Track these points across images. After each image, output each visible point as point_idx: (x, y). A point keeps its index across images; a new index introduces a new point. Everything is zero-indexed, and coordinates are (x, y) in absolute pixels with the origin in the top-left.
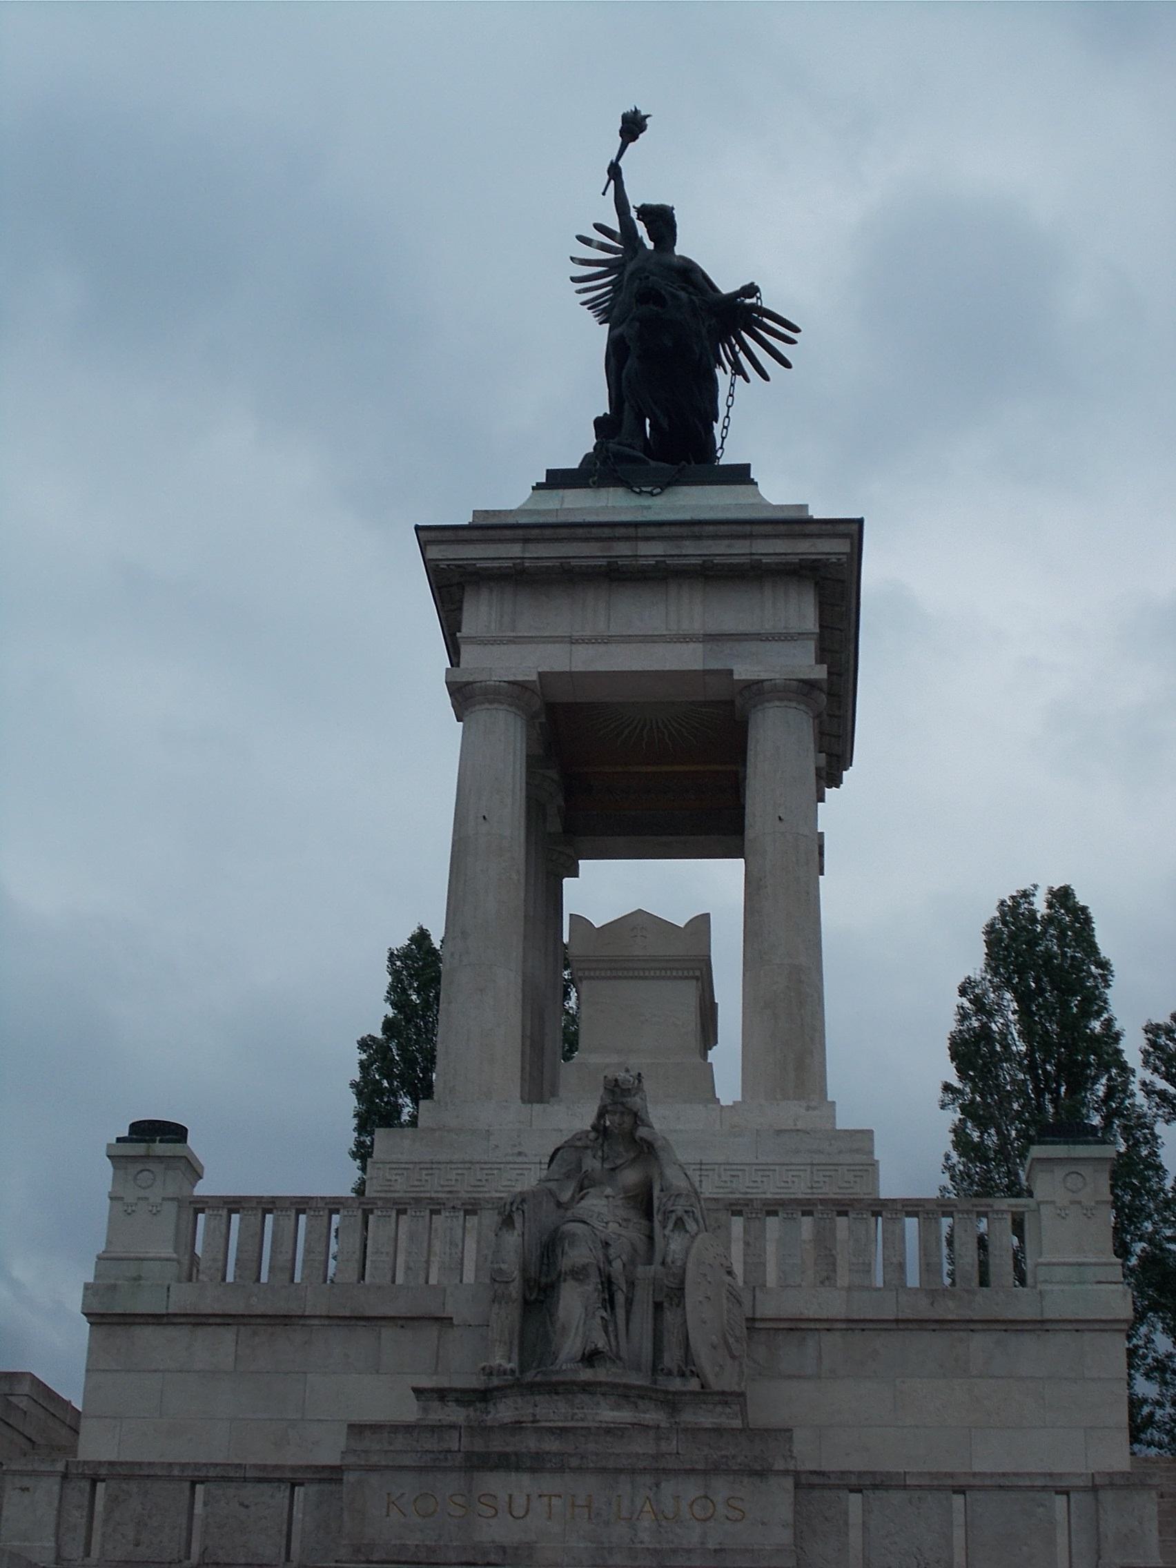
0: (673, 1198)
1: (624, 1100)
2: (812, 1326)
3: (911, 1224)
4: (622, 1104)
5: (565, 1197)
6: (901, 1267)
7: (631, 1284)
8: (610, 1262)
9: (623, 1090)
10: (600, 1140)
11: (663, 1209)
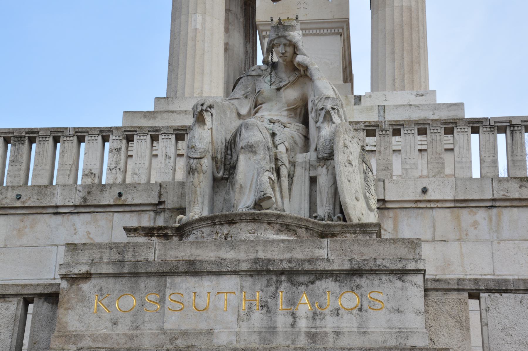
0: (323, 99)
1: (286, 33)
3: (501, 138)
4: (284, 37)
5: (244, 111)
6: (495, 162)
7: (293, 164)
8: (276, 147)
9: (284, 26)
10: (269, 70)
11: (315, 108)
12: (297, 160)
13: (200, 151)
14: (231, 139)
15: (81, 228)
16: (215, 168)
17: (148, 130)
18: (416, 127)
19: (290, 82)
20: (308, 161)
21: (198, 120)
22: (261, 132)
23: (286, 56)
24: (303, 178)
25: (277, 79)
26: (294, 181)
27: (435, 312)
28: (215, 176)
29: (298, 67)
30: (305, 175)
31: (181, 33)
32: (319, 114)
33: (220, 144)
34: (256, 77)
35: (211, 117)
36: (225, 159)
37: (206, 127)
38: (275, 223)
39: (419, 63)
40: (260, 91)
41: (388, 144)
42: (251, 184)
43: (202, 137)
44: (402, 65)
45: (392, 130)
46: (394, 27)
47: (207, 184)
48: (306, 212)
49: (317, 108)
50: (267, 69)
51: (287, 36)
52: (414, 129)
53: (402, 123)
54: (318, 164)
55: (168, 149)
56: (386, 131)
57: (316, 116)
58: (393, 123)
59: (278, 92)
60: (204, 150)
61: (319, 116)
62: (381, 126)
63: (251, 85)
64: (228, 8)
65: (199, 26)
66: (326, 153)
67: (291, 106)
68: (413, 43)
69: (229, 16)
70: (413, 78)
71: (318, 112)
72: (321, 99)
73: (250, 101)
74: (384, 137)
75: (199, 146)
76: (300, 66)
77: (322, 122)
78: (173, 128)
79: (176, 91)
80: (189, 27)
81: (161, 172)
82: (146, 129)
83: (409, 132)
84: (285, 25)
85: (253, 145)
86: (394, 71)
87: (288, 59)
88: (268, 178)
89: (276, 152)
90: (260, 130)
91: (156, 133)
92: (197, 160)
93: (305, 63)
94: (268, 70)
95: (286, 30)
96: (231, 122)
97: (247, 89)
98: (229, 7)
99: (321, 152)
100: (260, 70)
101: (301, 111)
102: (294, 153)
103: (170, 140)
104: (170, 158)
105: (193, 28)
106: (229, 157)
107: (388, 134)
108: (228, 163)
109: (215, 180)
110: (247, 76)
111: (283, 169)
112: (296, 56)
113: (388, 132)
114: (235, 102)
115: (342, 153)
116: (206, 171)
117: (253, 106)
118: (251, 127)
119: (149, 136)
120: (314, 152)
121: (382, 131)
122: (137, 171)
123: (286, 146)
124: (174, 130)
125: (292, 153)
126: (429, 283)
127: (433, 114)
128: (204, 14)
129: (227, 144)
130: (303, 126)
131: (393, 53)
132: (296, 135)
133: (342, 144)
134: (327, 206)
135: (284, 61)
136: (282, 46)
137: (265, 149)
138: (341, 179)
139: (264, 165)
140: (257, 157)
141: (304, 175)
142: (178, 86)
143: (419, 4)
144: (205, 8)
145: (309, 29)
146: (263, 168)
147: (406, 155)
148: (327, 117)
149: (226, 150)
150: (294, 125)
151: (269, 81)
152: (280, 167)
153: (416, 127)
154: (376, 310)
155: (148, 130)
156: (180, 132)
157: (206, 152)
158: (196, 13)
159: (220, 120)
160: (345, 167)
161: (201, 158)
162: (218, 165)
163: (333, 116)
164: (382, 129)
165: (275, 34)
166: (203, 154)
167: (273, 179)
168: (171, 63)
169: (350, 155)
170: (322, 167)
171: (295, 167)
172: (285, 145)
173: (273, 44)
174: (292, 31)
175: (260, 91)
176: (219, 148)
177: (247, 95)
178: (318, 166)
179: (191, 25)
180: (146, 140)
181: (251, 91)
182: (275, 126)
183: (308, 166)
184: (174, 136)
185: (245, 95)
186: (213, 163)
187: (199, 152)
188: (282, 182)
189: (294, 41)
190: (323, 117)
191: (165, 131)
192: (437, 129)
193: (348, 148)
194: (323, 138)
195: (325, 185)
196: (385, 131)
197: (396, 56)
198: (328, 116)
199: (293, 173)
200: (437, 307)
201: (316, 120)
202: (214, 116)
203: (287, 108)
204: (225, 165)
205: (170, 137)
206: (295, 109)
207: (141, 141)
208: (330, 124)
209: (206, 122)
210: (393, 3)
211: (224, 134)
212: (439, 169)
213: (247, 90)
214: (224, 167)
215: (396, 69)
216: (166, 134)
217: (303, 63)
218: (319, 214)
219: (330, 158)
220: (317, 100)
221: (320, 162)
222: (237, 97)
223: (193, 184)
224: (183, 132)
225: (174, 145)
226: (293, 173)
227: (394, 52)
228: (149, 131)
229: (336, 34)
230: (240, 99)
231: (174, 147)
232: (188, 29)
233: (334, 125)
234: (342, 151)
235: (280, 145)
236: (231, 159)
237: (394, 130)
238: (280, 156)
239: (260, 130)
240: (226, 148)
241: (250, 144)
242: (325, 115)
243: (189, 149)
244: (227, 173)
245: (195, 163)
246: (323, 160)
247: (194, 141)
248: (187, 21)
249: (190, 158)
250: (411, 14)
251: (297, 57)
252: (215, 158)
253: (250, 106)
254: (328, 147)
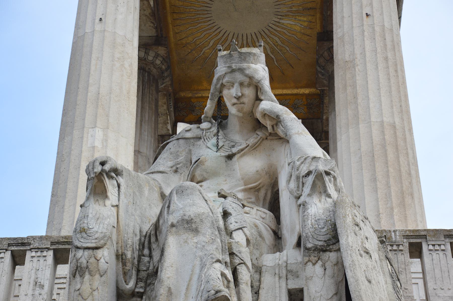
0: (309, 160)
1: (245, 65)
4: (241, 70)
7: (258, 270)
8: (230, 234)
10: (214, 129)
12: (265, 263)
13: (96, 236)
14: (149, 231)
16: (121, 273)
17: (9, 244)
18: (446, 241)
19: (248, 145)
20: (285, 264)
21: (95, 190)
22: (206, 200)
23: (244, 103)
24: (277, 291)
25: (227, 142)
26: (260, 297)
28: (121, 288)
29: (262, 121)
30: (280, 287)
31: (72, 152)
32: (303, 184)
33: (131, 235)
34: (192, 141)
35: (117, 188)
36: (139, 261)
37: (108, 203)
39: (412, 195)
40: (199, 159)
41: (403, 266)
43: (101, 216)
44: (388, 196)
45: (407, 245)
46: (373, 147)
47: (106, 295)
49: (299, 173)
50: (210, 128)
51: (245, 69)
52: (444, 243)
53: (423, 233)
54: (307, 258)
55: (39, 272)
56: (398, 245)
57: (298, 187)
58: (408, 233)
59: (230, 162)
60: (103, 235)
61: (303, 186)
62: (389, 238)
63: (184, 153)
64: (138, 149)
65: (98, 144)
66: (320, 241)
68: (402, 169)
69: (138, 158)
70: (406, 214)
71: (301, 180)
72: (305, 159)
73: (182, 177)
74: (395, 255)
75: (95, 229)
76: (267, 118)
77: (309, 195)
78: (51, 240)
79: (60, 229)
80: (84, 143)
82: (5, 243)
83: (437, 247)
84: (241, 53)
85: (192, 219)
86: (378, 204)
87: (247, 108)
88: (220, 273)
89: (230, 243)
90: (204, 197)
91: (22, 249)
92: (91, 251)
93: (276, 110)
94: (211, 130)
95: (243, 60)
96: (150, 205)
97: (178, 158)
98: (139, 148)
99: (310, 239)
100: (199, 130)
101: (266, 194)
102: (259, 252)
103: (44, 259)
104: (42, 287)
105: (89, 145)
106: (146, 259)
107: (401, 250)
108: (145, 269)
110: (178, 139)
111: (242, 271)
112: (259, 104)
113: (401, 248)
114: (158, 177)
115: (353, 234)
116: (106, 272)
118: (189, 191)
119: (8, 254)
120: (294, 250)
121: (392, 246)
123: (246, 236)
124: (52, 243)
125: (255, 251)
128: (106, 128)
129: (143, 239)
130: (271, 214)
131: (374, 180)
133: (350, 220)
135: (239, 111)
136: (236, 85)
137: (214, 228)
138: (355, 275)
139: (212, 252)
140: (201, 238)
141: (277, 285)
142: (64, 221)
143: (405, 122)
144: (108, 121)
146: (211, 256)
147: (436, 284)
148: (318, 186)
149: (141, 247)
150: (257, 210)
151: (214, 146)
152: (238, 267)
153: (448, 240)
155: (9, 244)
156: (61, 247)
157: (106, 238)
158: (95, 127)
159: (132, 197)
160: (360, 257)
161: (97, 248)
162: (127, 268)
163: (327, 185)
164: (392, 242)
165: (225, 67)
166: (102, 242)
168: (54, 194)
169: (366, 241)
170: (314, 264)
171: (260, 274)
172: (245, 234)
173: (222, 84)
174: (253, 61)
175: (199, 159)
176: (130, 240)
177: (177, 168)
178: (307, 262)
179: (87, 142)
181: (184, 162)
182: (228, 201)
183: (284, 272)
184: (51, 253)
185: (174, 168)
186: (117, 265)
187: (94, 238)
188: (241, 291)
190: (310, 187)
191: (36, 245)
193: (360, 229)
194: (313, 217)
195: (321, 295)
197: (378, 183)
198: (319, 183)
199: (258, 284)
201: (298, 194)
202: (122, 188)
203: (243, 187)
204: (138, 271)
205: (45, 253)
206: (256, 190)
208: (323, 197)
209: (109, 194)
210: (370, 118)
211: (139, 221)
213: (178, 160)
214: (137, 275)
215: (379, 200)
216: (38, 248)
217: (271, 112)
219: (328, 248)
220: (298, 160)
221: (310, 256)
222: (161, 169)
223: (80, 294)
224: (67, 246)
225: (50, 266)
226: (258, 284)
227: (375, 179)
228: (9, 245)
230: (166, 173)
231: (50, 269)
232: (82, 147)
233: (329, 200)
234: (352, 231)
235: (237, 231)
236: (149, 262)
237: (411, 244)
238: (237, 250)
239: (204, 197)
240: (142, 245)
241: (186, 218)
242: (314, 182)
243: (76, 234)
244: (142, 284)
245: (86, 257)
246: (316, 252)
247: (85, 222)
248: (82, 138)
250: (395, 133)
252: (122, 255)
254: (325, 230)
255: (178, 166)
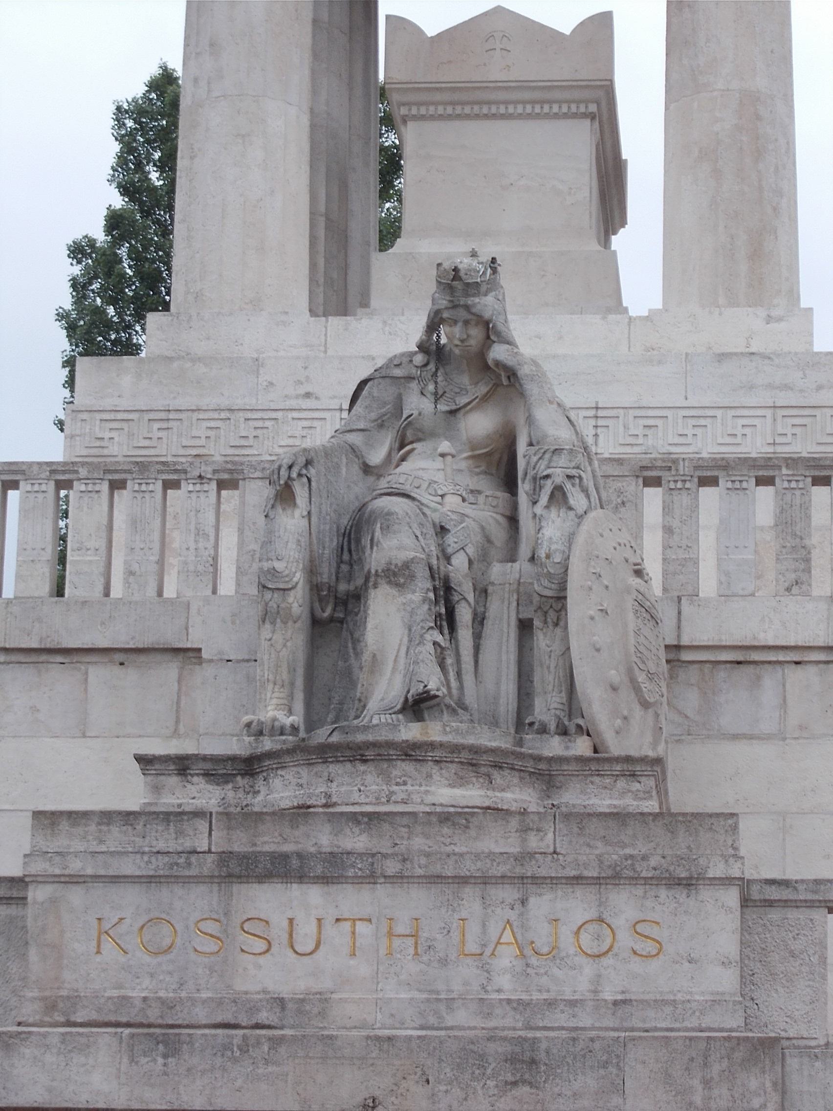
2: (772, 657)
4: (467, 308)
7: (483, 592)
10: (432, 367)
11: (531, 473)
15: (18, 698)
27: (763, 946)
34: (403, 380)
38: (446, 761)
42: (396, 656)
48: (510, 700)
52: (747, 478)
57: (534, 490)
61: (540, 490)
67: (481, 449)
72: (544, 453)
81: (188, 571)
94: (429, 367)
103: (206, 494)
109: (315, 622)
113: (688, 485)
117: (397, 445)
122: (135, 567)
126: (755, 888)
127: (802, 376)
129: (341, 539)
132: (491, 521)
134: (554, 694)
136: (460, 324)
145: (515, 103)
154: (646, 957)
163: (569, 495)
167: (443, 644)
172: (467, 554)
180: (153, 494)
185: (379, 421)
189: (487, 315)
192: (797, 481)
196: (682, 481)
200: (768, 936)
203: (470, 454)
205: (206, 487)
207: (141, 495)
209: (299, 501)
212: (799, 574)
218: (539, 717)
226: (482, 609)
229: (584, 116)
235: (457, 554)
249: (264, 587)
251: (492, 349)
253: (391, 444)
255: (384, 418)
